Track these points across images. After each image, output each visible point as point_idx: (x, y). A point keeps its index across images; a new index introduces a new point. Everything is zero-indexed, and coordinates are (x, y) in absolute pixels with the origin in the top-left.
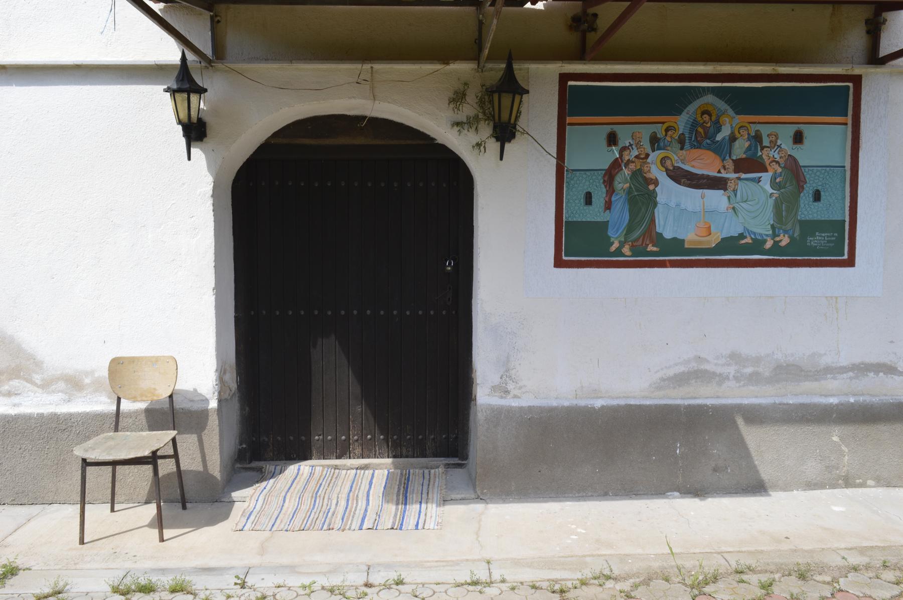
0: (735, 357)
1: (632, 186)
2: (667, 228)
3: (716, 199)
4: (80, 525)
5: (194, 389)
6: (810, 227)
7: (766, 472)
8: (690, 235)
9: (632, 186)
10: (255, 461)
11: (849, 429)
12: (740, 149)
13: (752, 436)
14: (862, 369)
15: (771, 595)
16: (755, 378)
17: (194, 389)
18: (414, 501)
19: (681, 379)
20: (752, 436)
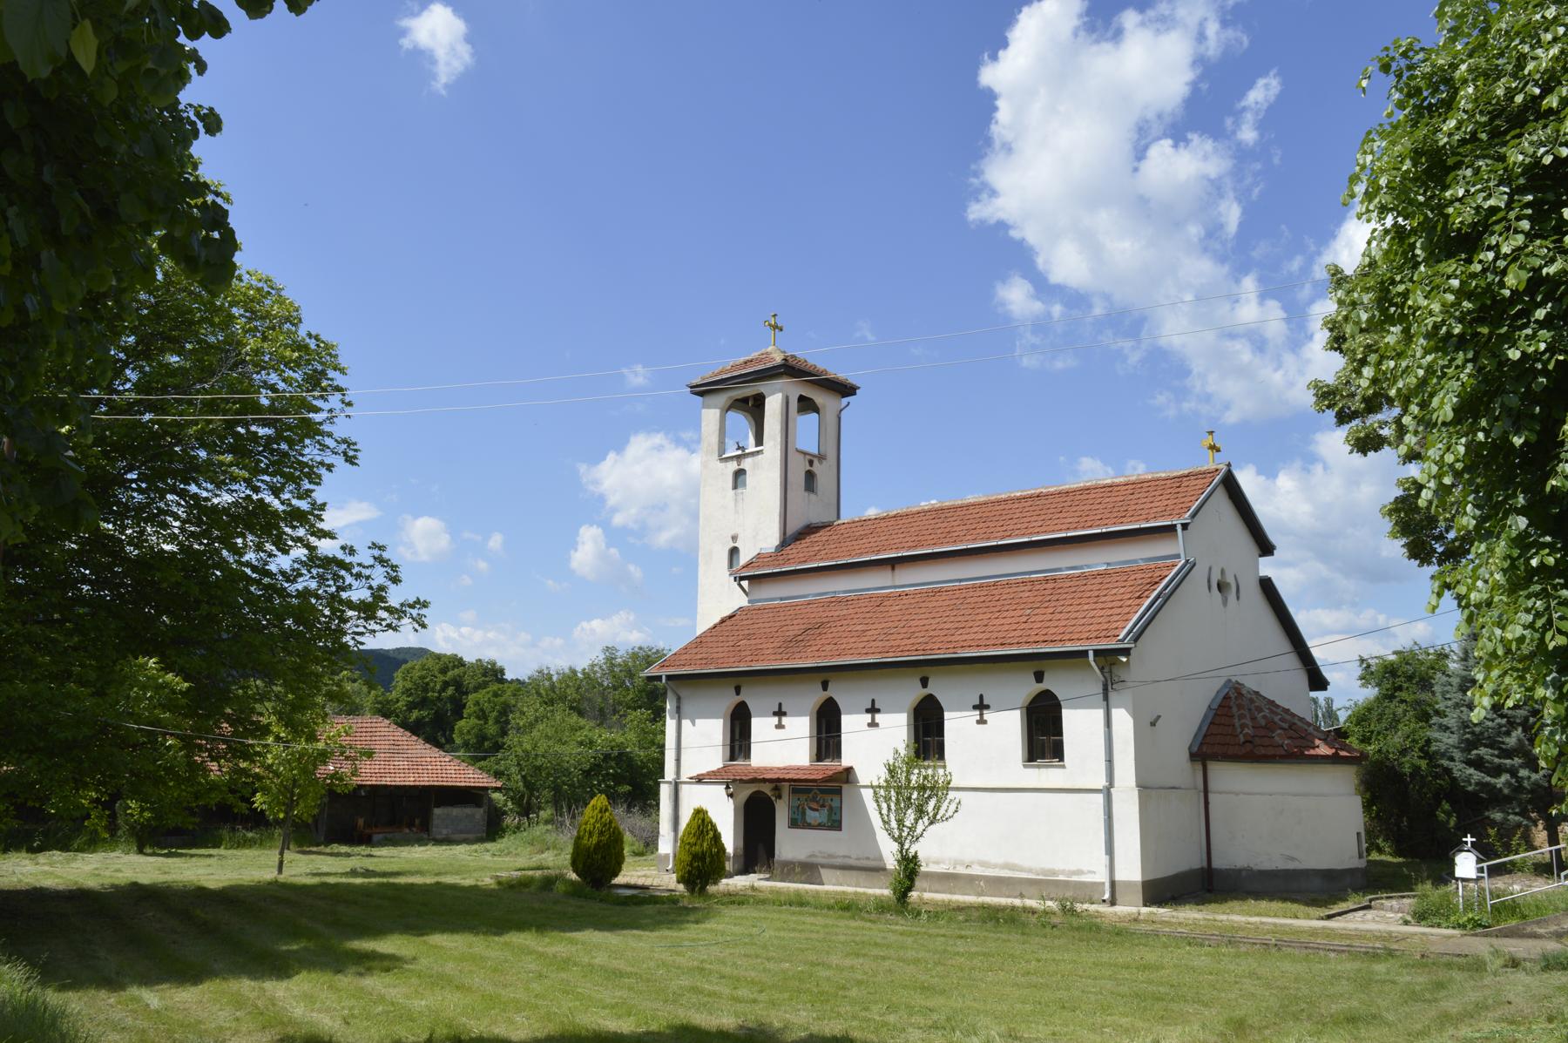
0: (820, 852)
1: (1439, 228)
2: (808, 820)
3: (817, 814)
4: (1032, 660)
5: (570, 668)
6: (834, 821)
7: (825, 881)
8: (813, 822)
9: (1439, 228)
10: (659, 1033)
11: (842, 871)
12: (821, 802)
13: (822, 871)
14: (844, 857)
15: (395, 597)
16: (824, 857)
17: (570, 668)
18: (79, 18)
19: (810, 856)
20: (822, 871)
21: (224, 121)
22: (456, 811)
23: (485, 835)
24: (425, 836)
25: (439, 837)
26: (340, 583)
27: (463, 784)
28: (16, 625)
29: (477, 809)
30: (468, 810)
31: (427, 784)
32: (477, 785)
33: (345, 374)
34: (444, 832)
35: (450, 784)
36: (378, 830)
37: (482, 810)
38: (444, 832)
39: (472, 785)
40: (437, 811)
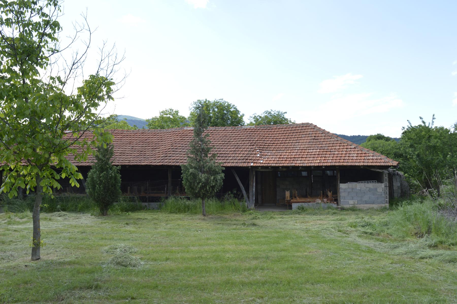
21: (166, 107)
22: (360, 186)
23: (387, 205)
24: (335, 206)
25: (346, 206)
26: (450, 147)
27: (362, 164)
28: (150, 249)
29: (380, 184)
30: (371, 185)
31: (329, 164)
32: (373, 164)
33: (114, 100)
34: (351, 202)
35: (350, 164)
36: (295, 200)
37: (383, 185)
38: (351, 202)
39: (371, 164)
40: (342, 186)
